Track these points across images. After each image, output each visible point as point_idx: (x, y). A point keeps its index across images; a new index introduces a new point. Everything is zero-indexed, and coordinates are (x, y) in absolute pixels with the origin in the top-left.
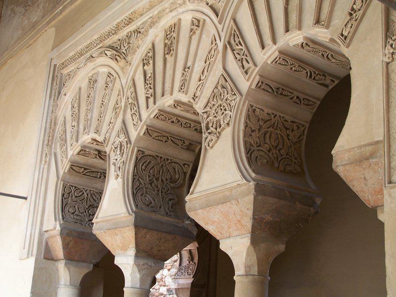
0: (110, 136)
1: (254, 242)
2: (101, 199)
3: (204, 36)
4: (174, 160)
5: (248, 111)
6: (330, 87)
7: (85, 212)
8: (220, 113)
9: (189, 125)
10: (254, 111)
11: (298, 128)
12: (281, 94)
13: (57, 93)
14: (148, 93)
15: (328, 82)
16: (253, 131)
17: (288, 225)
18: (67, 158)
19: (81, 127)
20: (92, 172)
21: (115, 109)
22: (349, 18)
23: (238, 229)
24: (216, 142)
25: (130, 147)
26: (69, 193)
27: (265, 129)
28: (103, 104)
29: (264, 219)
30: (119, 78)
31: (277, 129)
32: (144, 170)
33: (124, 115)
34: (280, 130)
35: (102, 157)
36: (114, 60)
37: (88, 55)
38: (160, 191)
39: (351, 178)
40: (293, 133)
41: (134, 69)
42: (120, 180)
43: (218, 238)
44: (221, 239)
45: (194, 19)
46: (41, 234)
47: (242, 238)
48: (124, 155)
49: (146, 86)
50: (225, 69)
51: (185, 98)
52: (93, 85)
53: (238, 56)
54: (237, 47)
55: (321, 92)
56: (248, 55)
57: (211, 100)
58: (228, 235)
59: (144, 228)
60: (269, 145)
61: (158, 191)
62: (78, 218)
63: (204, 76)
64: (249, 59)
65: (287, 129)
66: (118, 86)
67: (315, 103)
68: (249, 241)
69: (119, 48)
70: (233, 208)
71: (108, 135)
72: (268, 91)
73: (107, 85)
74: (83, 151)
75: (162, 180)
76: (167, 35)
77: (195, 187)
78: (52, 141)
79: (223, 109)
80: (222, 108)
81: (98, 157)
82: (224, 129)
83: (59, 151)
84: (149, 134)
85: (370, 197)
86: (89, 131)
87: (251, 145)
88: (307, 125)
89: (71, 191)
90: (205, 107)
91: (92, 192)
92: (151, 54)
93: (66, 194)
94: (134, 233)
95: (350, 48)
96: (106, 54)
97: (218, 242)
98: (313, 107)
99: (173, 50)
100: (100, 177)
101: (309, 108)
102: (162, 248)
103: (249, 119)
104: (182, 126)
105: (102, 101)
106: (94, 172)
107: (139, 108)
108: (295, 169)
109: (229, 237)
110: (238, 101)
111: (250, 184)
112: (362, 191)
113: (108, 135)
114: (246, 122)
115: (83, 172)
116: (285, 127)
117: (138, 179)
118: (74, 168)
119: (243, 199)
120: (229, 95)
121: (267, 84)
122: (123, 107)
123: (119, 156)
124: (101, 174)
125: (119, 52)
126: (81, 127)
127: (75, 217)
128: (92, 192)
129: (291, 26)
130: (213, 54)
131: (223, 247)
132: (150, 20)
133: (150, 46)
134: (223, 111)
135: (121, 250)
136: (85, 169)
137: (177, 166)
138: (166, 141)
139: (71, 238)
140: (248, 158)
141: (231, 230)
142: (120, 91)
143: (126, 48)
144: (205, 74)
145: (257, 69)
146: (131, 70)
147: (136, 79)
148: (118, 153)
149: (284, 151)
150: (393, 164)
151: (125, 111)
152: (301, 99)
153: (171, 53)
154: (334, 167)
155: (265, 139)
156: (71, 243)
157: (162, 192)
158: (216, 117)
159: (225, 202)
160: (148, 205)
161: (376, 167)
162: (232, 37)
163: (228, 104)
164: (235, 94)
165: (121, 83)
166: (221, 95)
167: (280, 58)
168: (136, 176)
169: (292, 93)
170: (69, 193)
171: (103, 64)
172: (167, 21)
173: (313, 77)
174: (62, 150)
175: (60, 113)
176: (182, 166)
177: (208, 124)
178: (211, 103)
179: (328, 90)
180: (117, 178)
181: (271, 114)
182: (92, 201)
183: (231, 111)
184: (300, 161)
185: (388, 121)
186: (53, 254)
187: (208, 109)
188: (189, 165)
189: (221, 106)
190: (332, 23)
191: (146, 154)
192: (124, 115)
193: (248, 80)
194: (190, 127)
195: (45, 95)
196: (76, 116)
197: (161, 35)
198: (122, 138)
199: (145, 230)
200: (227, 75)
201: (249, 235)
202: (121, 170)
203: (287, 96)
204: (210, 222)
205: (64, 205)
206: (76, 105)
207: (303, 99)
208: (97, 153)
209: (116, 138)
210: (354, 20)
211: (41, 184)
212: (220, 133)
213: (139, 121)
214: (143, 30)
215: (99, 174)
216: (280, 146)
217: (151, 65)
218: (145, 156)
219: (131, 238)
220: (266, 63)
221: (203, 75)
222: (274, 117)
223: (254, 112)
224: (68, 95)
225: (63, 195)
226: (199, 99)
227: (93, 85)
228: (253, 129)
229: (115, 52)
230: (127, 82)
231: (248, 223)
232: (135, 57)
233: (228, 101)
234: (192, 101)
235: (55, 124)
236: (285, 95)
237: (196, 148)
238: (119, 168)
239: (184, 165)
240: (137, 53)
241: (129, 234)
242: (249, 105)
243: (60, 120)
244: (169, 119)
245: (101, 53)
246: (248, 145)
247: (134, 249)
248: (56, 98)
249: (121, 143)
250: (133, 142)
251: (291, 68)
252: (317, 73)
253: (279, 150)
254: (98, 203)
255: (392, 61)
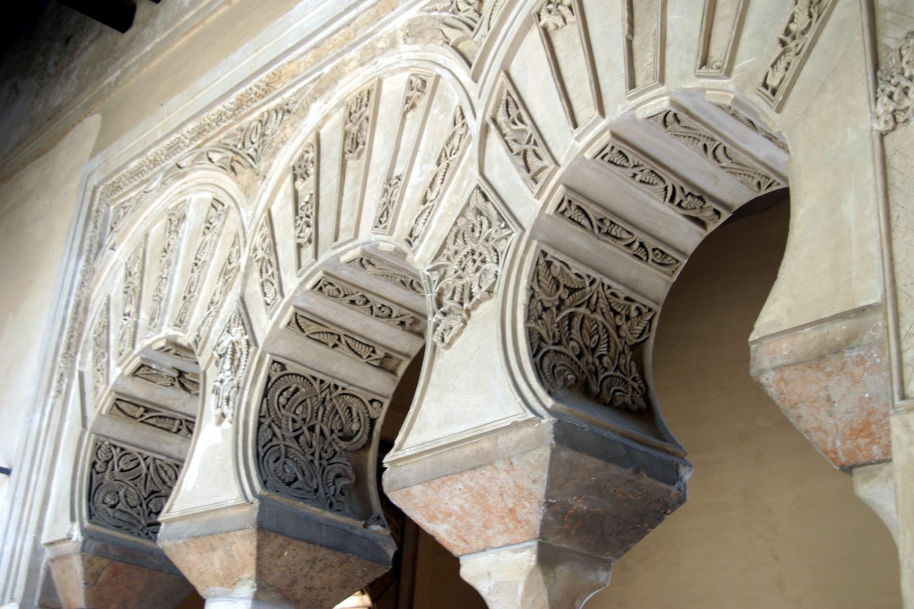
0: (209, 333)
1: (547, 558)
2: (176, 478)
3: (434, 111)
4: (350, 390)
5: (537, 264)
6: (711, 228)
7: (141, 505)
8: (471, 268)
9: (387, 312)
10: (549, 264)
11: (640, 313)
12: (608, 233)
13: (95, 246)
14: (301, 235)
15: (707, 215)
16: (545, 309)
17: (619, 524)
18: (108, 382)
19: (144, 316)
20: (160, 417)
21: (224, 272)
22: (780, 49)
23: (507, 531)
24: (459, 334)
25: (255, 352)
26: (107, 462)
27: (570, 307)
28: (196, 264)
29: (570, 507)
30: (238, 208)
31: (594, 311)
32: (284, 406)
33: (244, 285)
34: (603, 314)
35: (187, 385)
36: (229, 170)
37: (171, 162)
38: (317, 455)
39: (795, 398)
40: (629, 323)
41: (274, 191)
42: (227, 425)
43: (456, 552)
44: (464, 555)
45: (413, 78)
46: (36, 551)
47: (516, 552)
48: (240, 371)
49: (299, 222)
50: (482, 174)
51: (387, 244)
52: (177, 226)
53: (515, 147)
54: (514, 127)
55: (688, 237)
56: (539, 141)
57: (450, 242)
58: (481, 544)
59: (279, 532)
60: (578, 343)
61: (313, 454)
62: (125, 517)
63: (435, 193)
64: (541, 150)
65: (616, 313)
66: (232, 225)
67: (678, 261)
68: (534, 558)
69: (240, 146)
70: (497, 480)
71: (205, 329)
72: (579, 224)
73: (208, 225)
74: (143, 371)
75: (322, 433)
76: (350, 114)
77: (407, 434)
78: (77, 347)
79: (479, 260)
80: (475, 257)
81: (177, 384)
82: (479, 302)
83: (88, 369)
84: (300, 327)
85: (838, 443)
86: (162, 324)
87: (541, 339)
88: (658, 309)
89: (112, 458)
90: (436, 258)
91: (158, 462)
92: (312, 155)
93: (99, 463)
94: (255, 543)
95: (785, 111)
96: (210, 160)
97: (455, 563)
98: (673, 268)
99: (364, 144)
100: (179, 430)
101: (663, 272)
102: (317, 583)
103: (538, 281)
104: (372, 313)
105: (196, 258)
106: (165, 417)
107: (278, 269)
108: (634, 403)
109: (484, 550)
110: (515, 242)
111: (543, 421)
112: (819, 429)
113: (205, 329)
114: (532, 288)
115: (142, 416)
116: (612, 309)
117: (270, 426)
118: (123, 405)
119: (525, 457)
120: (493, 230)
121: (579, 208)
122: (242, 269)
123: (229, 373)
124: (181, 424)
125: (243, 157)
126: (144, 316)
127: (118, 515)
128: (158, 462)
129: (640, 80)
130: (456, 145)
131: (468, 572)
132: (312, 86)
133: (311, 139)
134: (478, 263)
135: (222, 585)
136: (147, 410)
137: (355, 405)
138: (335, 346)
139: (105, 562)
140: (536, 364)
141: (490, 532)
142: (237, 236)
143: (256, 146)
144: (436, 189)
145: (560, 172)
146: (265, 190)
147: (274, 209)
148: (227, 366)
149: (609, 361)
150: (907, 356)
151: (246, 277)
152: (650, 251)
153: (358, 150)
154: (753, 371)
155: (569, 329)
156: (105, 573)
157: (321, 458)
158: (460, 277)
159: (480, 466)
160: (289, 484)
161: (858, 371)
162: (502, 108)
163: (490, 248)
164: (507, 226)
165: (241, 218)
166: (473, 230)
167: (613, 148)
168: (264, 417)
169: (629, 233)
170: (107, 462)
171: (202, 184)
172: (351, 84)
173: (677, 201)
174: (99, 367)
175: (97, 288)
176: (368, 404)
177: (440, 294)
178: (449, 249)
179: (706, 234)
180: (219, 423)
181: (583, 275)
182: (160, 480)
183: (498, 263)
184: (642, 386)
185: (891, 259)
186: (61, 597)
187: (442, 261)
188: (382, 403)
189: (473, 254)
190: (737, 67)
191: (290, 370)
192: (244, 285)
193: (538, 196)
194: (390, 316)
195: (68, 250)
196: (133, 293)
197: (339, 115)
198: (238, 334)
199: (281, 540)
200: (486, 191)
201: (534, 544)
202: (231, 403)
203: (620, 239)
204: (441, 516)
205: (94, 486)
206: (135, 269)
207: (654, 250)
208: (176, 375)
209: (220, 335)
210: (792, 53)
211: (45, 442)
212: (468, 312)
213: (279, 296)
214: (297, 106)
215: (177, 422)
216: (602, 350)
217: (312, 178)
218: (287, 375)
219: (248, 557)
220: (580, 159)
221: (432, 191)
222: (591, 283)
223: (549, 267)
224: (119, 249)
225: (94, 464)
226: (421, 241)
227: (177, 226)
228: (547, 305)
229: (230, 154)
230: (254, 215)
231: (533, 514)
232: (275, 162)
233: (491, 243)
234: (405, 247)
235: (86, 310)
236: (615, 237)
237: (398, 365)
238: (228, 400)
239: (371, 401)
240: (280, 154)
241: (244, 547)
242: (539, 252)
243: (96, 307)
244: (345, 296)
245: (198, 158)
246: (535, 338)
247: (252, 582)
248: (92, 257)
249: (233, 344)
250: (261, 343)
251: (635, 175)
252: (687, 190)
253: (600, 357)
254: (171, 488)
255: (894, 129)
